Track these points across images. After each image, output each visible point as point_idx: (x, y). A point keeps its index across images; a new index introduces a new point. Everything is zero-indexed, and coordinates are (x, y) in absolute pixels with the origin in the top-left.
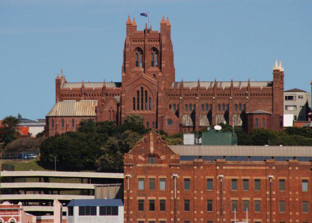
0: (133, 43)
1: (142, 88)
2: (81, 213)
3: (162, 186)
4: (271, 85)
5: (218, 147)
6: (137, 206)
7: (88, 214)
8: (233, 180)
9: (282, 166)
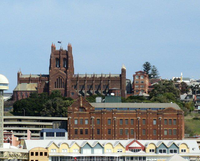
0: (54, 56)
1: (59, 77)
2: (47, 135)
3: (86, 122)
4: (121, 75)
5: (113, 104)
6: (74, 132)
7: (50, 136)
8: (121, 119)
9: (144, 112)
